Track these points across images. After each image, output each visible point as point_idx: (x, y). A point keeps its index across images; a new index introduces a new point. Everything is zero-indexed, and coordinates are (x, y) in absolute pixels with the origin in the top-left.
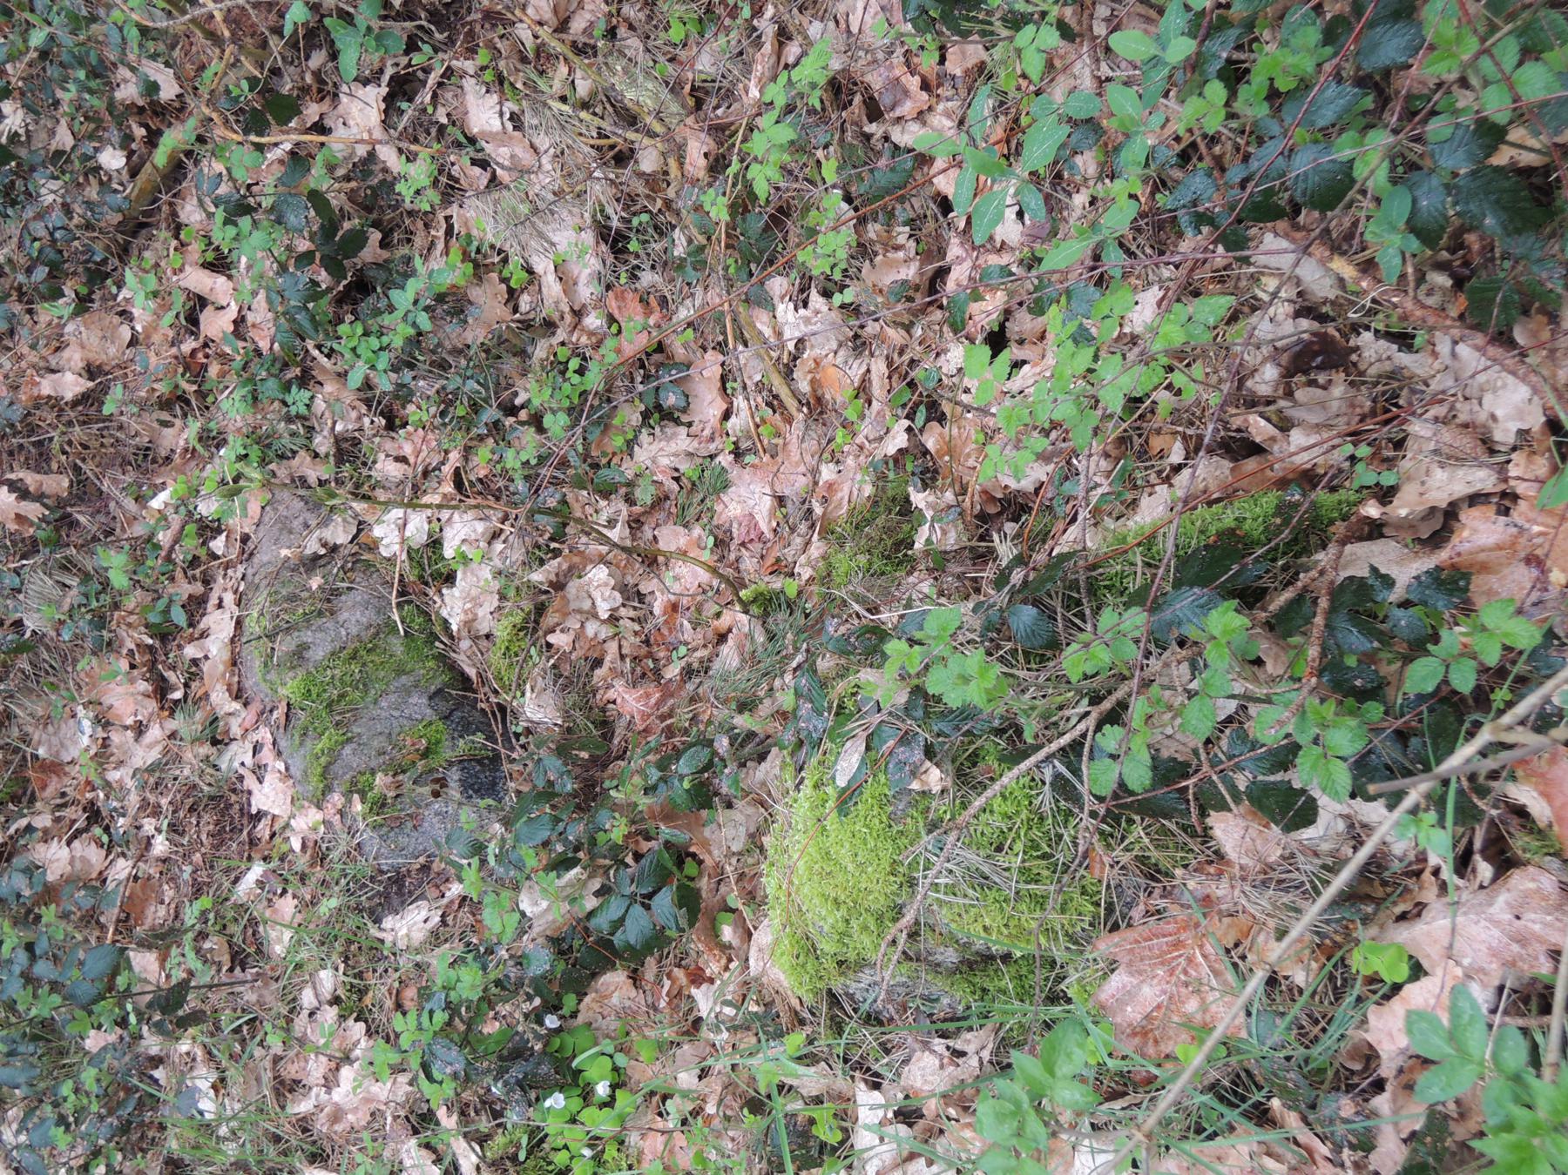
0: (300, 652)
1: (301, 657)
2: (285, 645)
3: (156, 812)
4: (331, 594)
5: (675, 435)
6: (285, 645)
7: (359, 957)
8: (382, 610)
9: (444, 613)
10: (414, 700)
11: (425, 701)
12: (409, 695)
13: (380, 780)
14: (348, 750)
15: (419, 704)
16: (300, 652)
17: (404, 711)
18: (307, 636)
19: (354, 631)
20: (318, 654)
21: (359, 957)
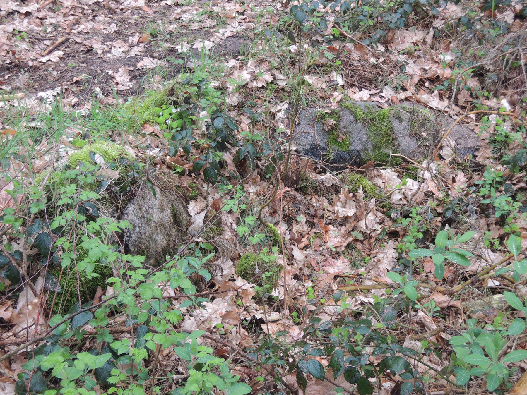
0: (399, 118)
1: (397, 118)
2: (405, 116)
3: (384, 62)
4: (418, 137)
5: (390, 265)
6: (405, 116)
7: (280, 94)
8: (404, 151)
9: (388, 170)
10: (360, 146)
11: (358, 149)
12: (363, 145)
13: (332, 122)
14: (352, 118)
15: (357, 146)
16: (399, 118)
17: (359, 140)
18: (405, 124)
19: (399, 139)
20: (396, 124)
21: (280, 94)
